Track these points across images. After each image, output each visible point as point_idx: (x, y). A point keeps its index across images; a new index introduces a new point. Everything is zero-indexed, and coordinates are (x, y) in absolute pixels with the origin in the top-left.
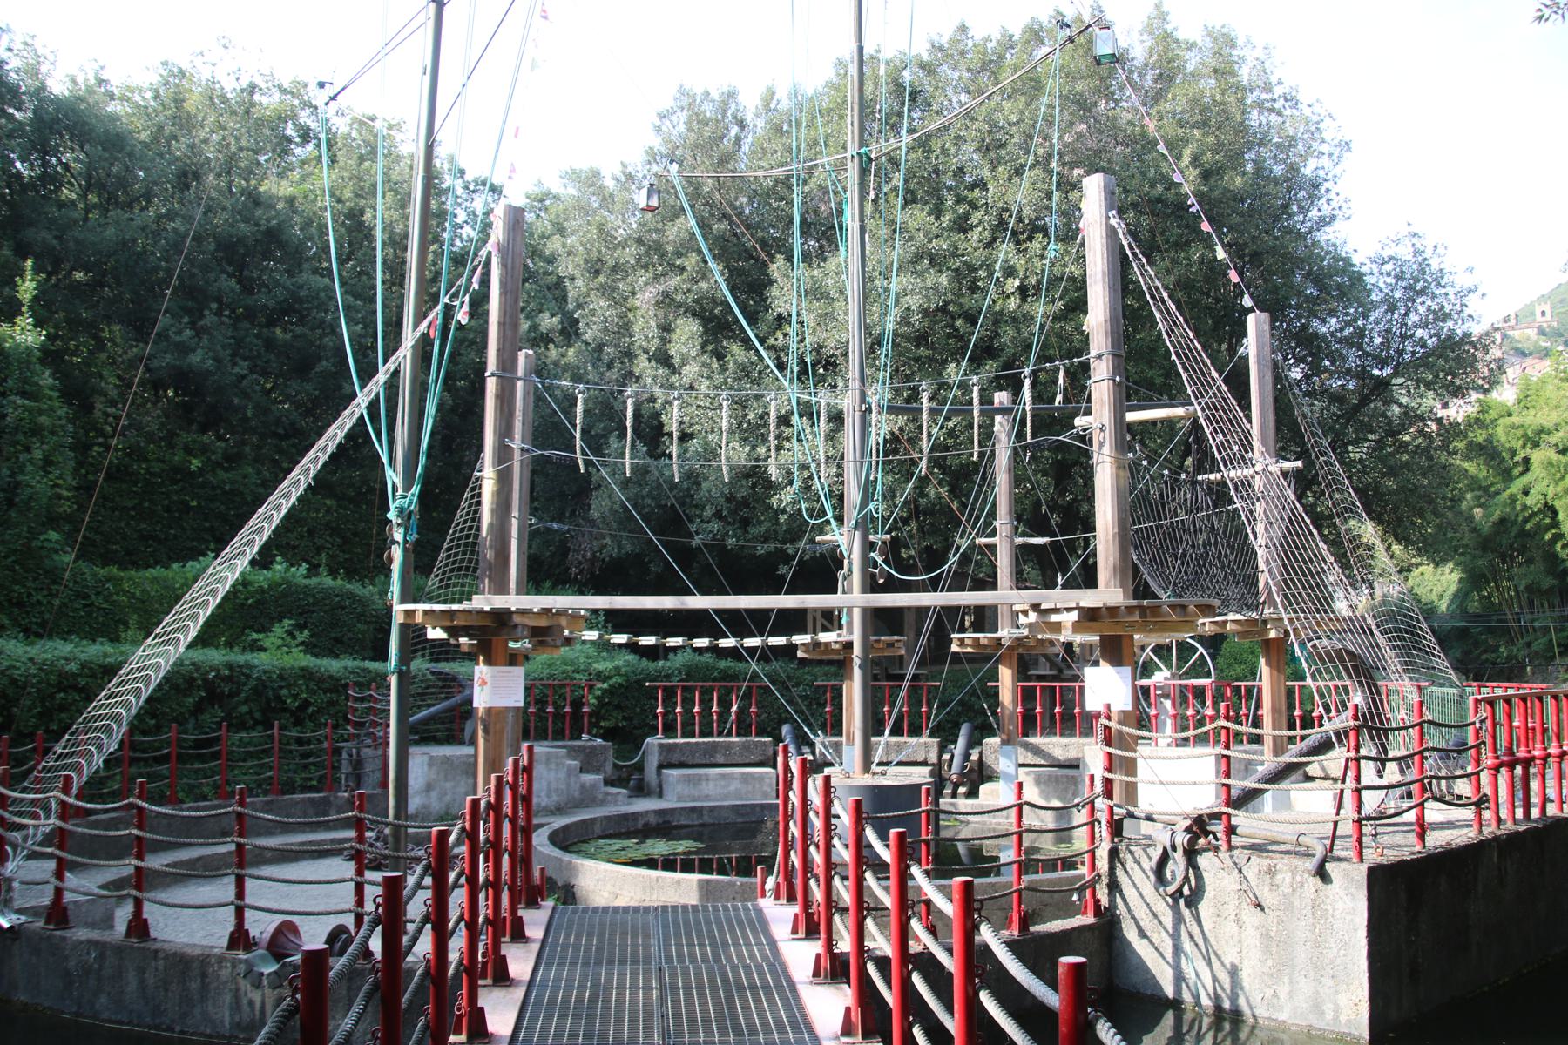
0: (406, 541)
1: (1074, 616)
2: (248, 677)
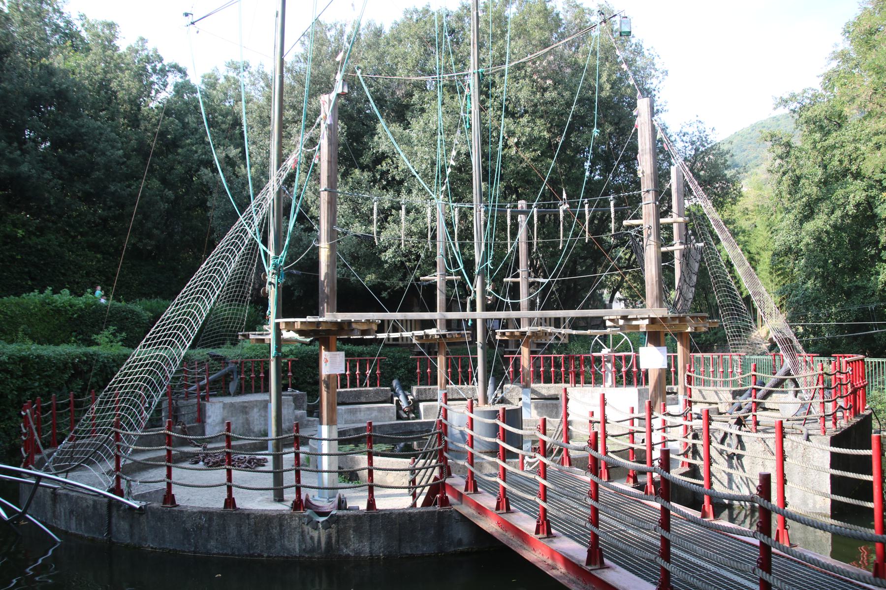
0: (278, 283)
1: (647, 322)
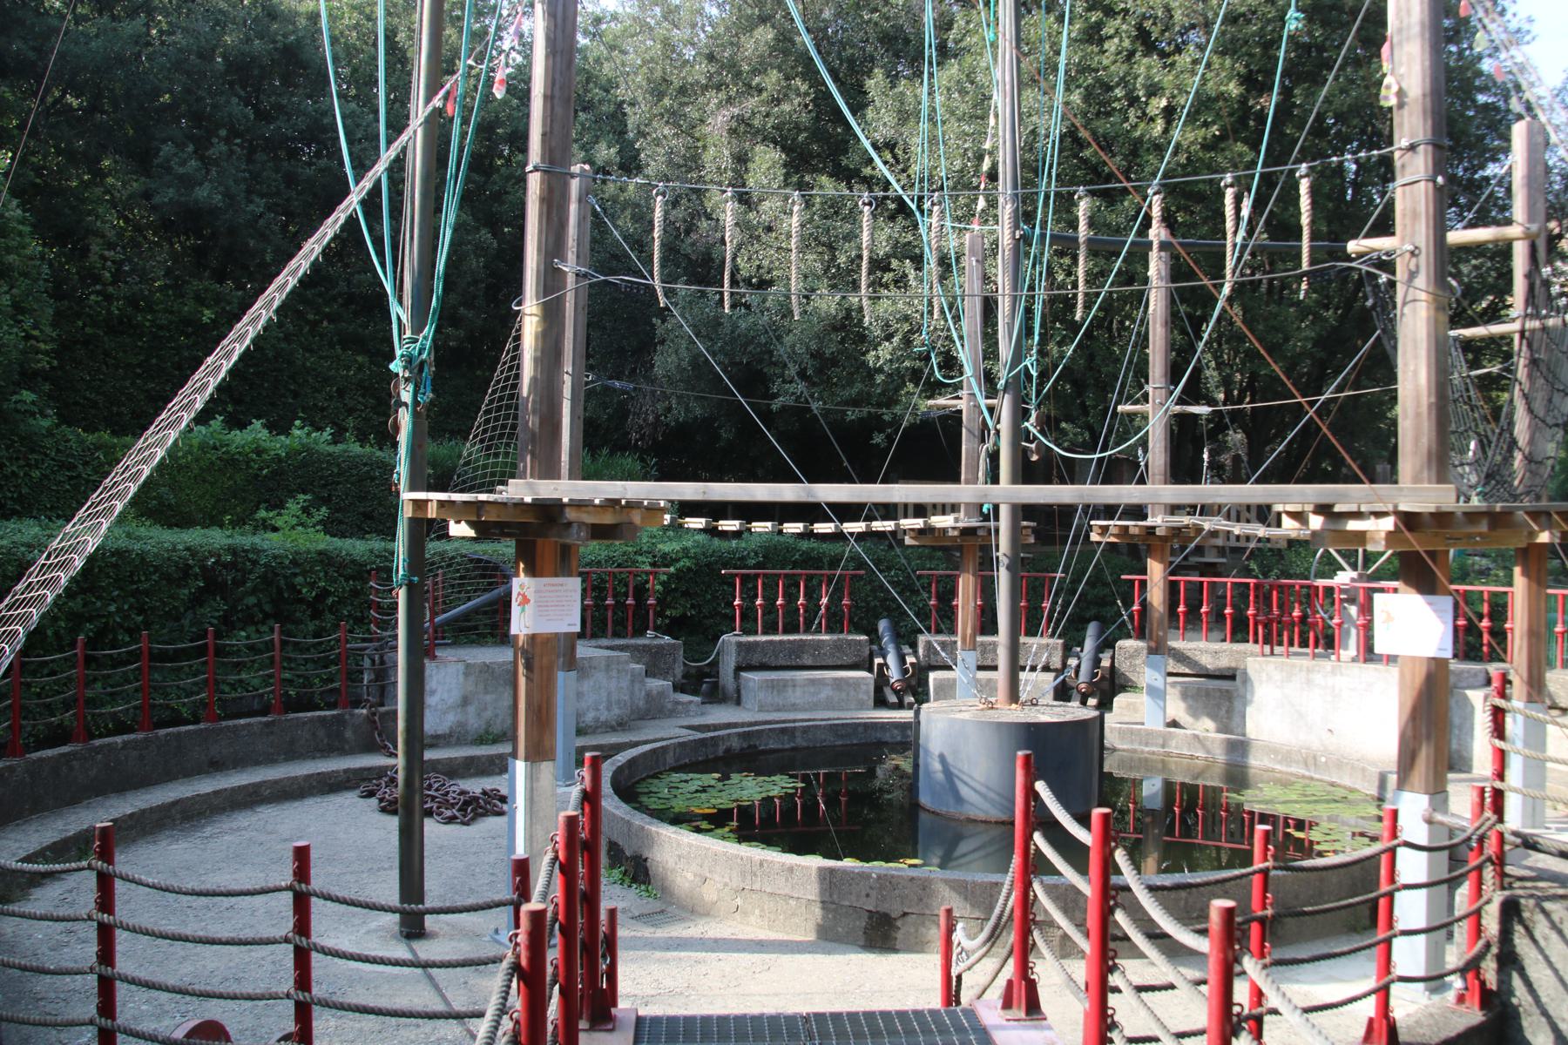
0: (416, 403)
1: (1388, 524)
2: (255, 562)
